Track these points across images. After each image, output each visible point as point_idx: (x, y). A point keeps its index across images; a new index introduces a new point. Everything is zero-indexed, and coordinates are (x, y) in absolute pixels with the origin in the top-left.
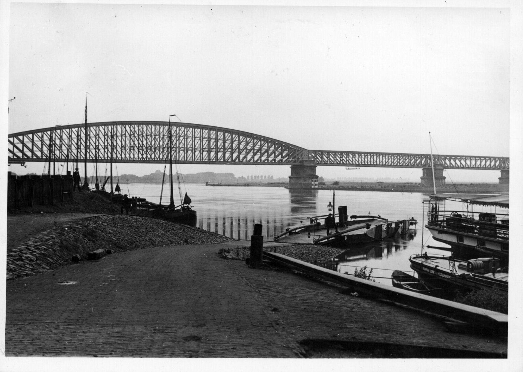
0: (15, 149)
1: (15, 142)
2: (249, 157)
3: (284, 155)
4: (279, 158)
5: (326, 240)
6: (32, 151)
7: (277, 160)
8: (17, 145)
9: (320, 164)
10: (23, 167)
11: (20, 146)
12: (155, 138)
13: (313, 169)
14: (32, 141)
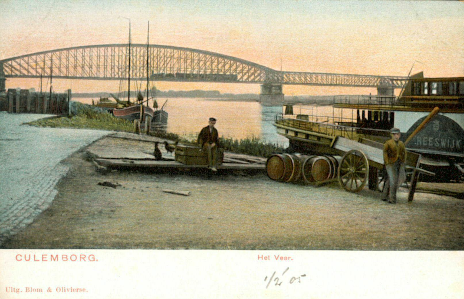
0: (29, 67)
1: (21, 63)
2: (245, 77)
3: (256, 75)
4: (252, 77)
5: (446, 164)
6: (36, 70)
7: (256, 79)
8: (16, 67)
9: (286, 83)
10: (216, 126)
11: (26, 66)
12: (153, 59)
13: (280, 88)
14: (36, 62)
